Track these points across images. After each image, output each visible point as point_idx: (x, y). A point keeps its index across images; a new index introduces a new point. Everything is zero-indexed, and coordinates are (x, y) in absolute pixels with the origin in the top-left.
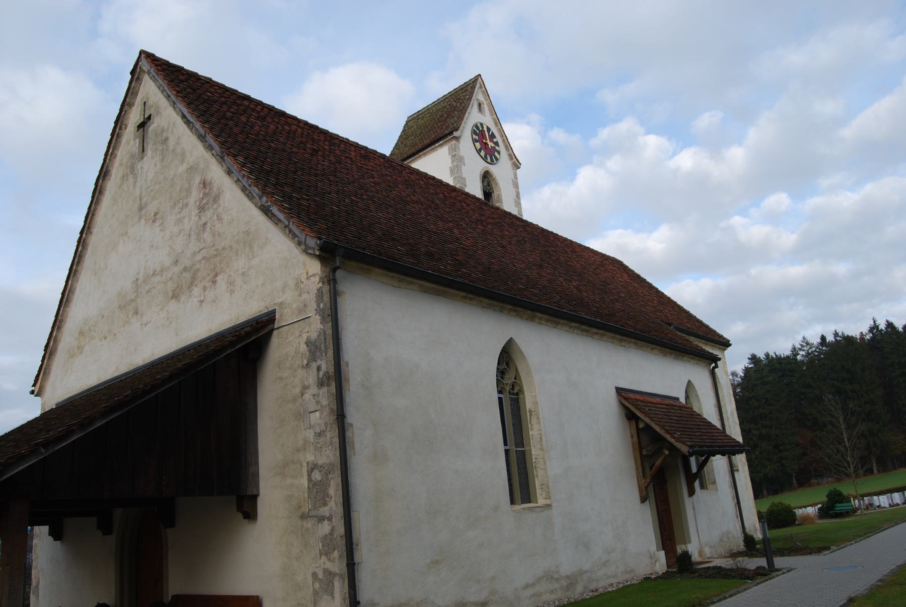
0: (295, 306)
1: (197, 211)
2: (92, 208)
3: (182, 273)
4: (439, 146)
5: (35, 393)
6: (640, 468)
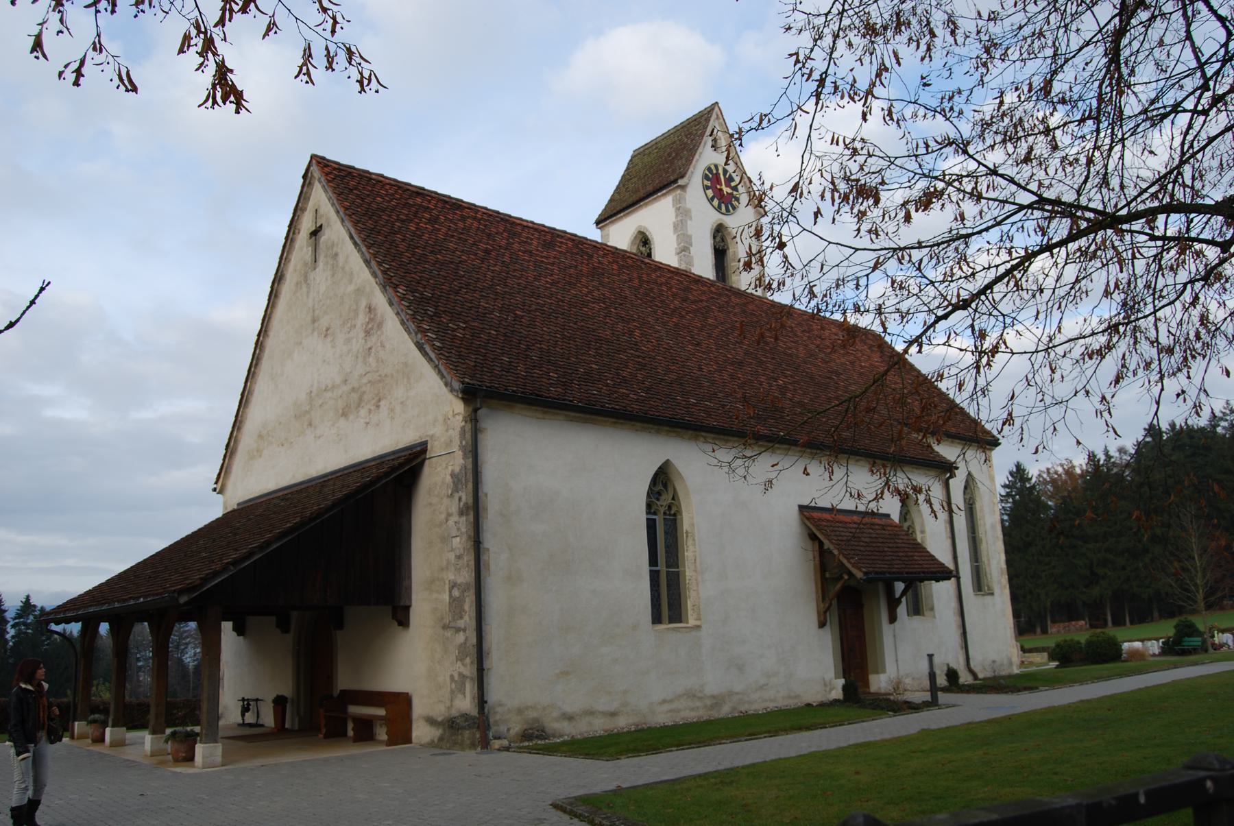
0: (443, 439)
1: (363, 335)
2: (268, 312)
4: (663, 195)
5: (218, 490)
6: (820, 591)
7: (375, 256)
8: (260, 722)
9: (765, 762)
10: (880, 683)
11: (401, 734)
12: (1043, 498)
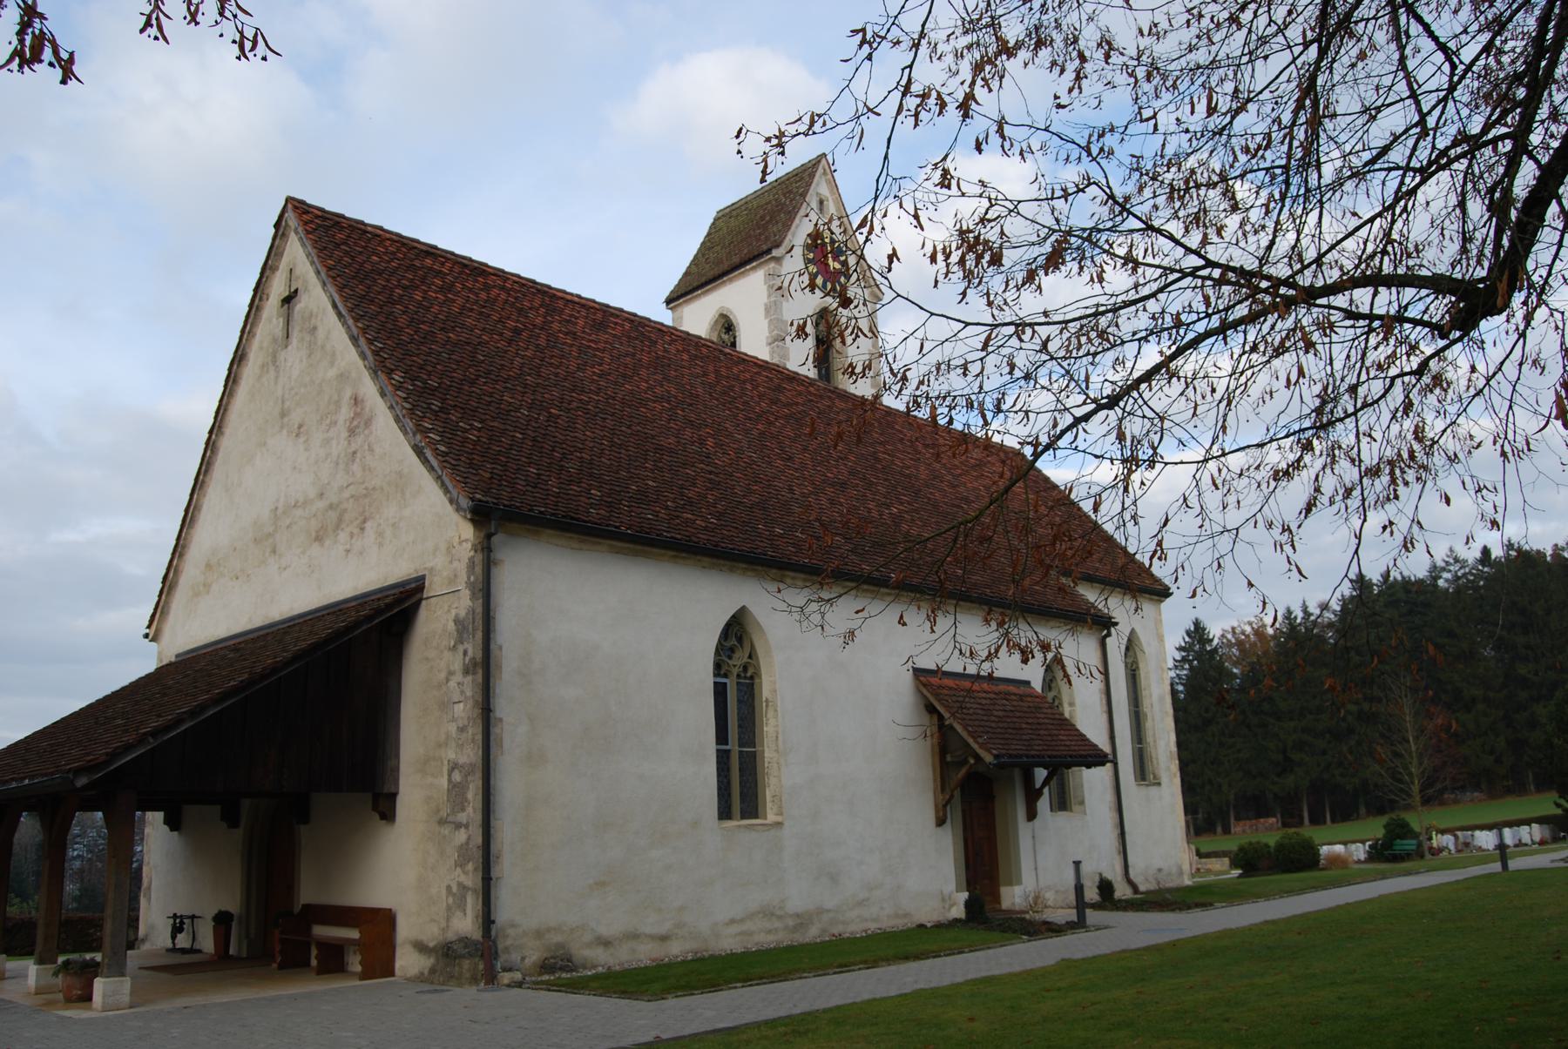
0: (445, 574)
1: (347, 434)
2: (224, 402)
3: (327, 511)
4: (752, 269)
5: (150, 637)
7: (364, 331)
8: (197, 946)
9: (854, 1003)
10: (1013, 897)
11: (380, 964)
12: (1226, 664)
